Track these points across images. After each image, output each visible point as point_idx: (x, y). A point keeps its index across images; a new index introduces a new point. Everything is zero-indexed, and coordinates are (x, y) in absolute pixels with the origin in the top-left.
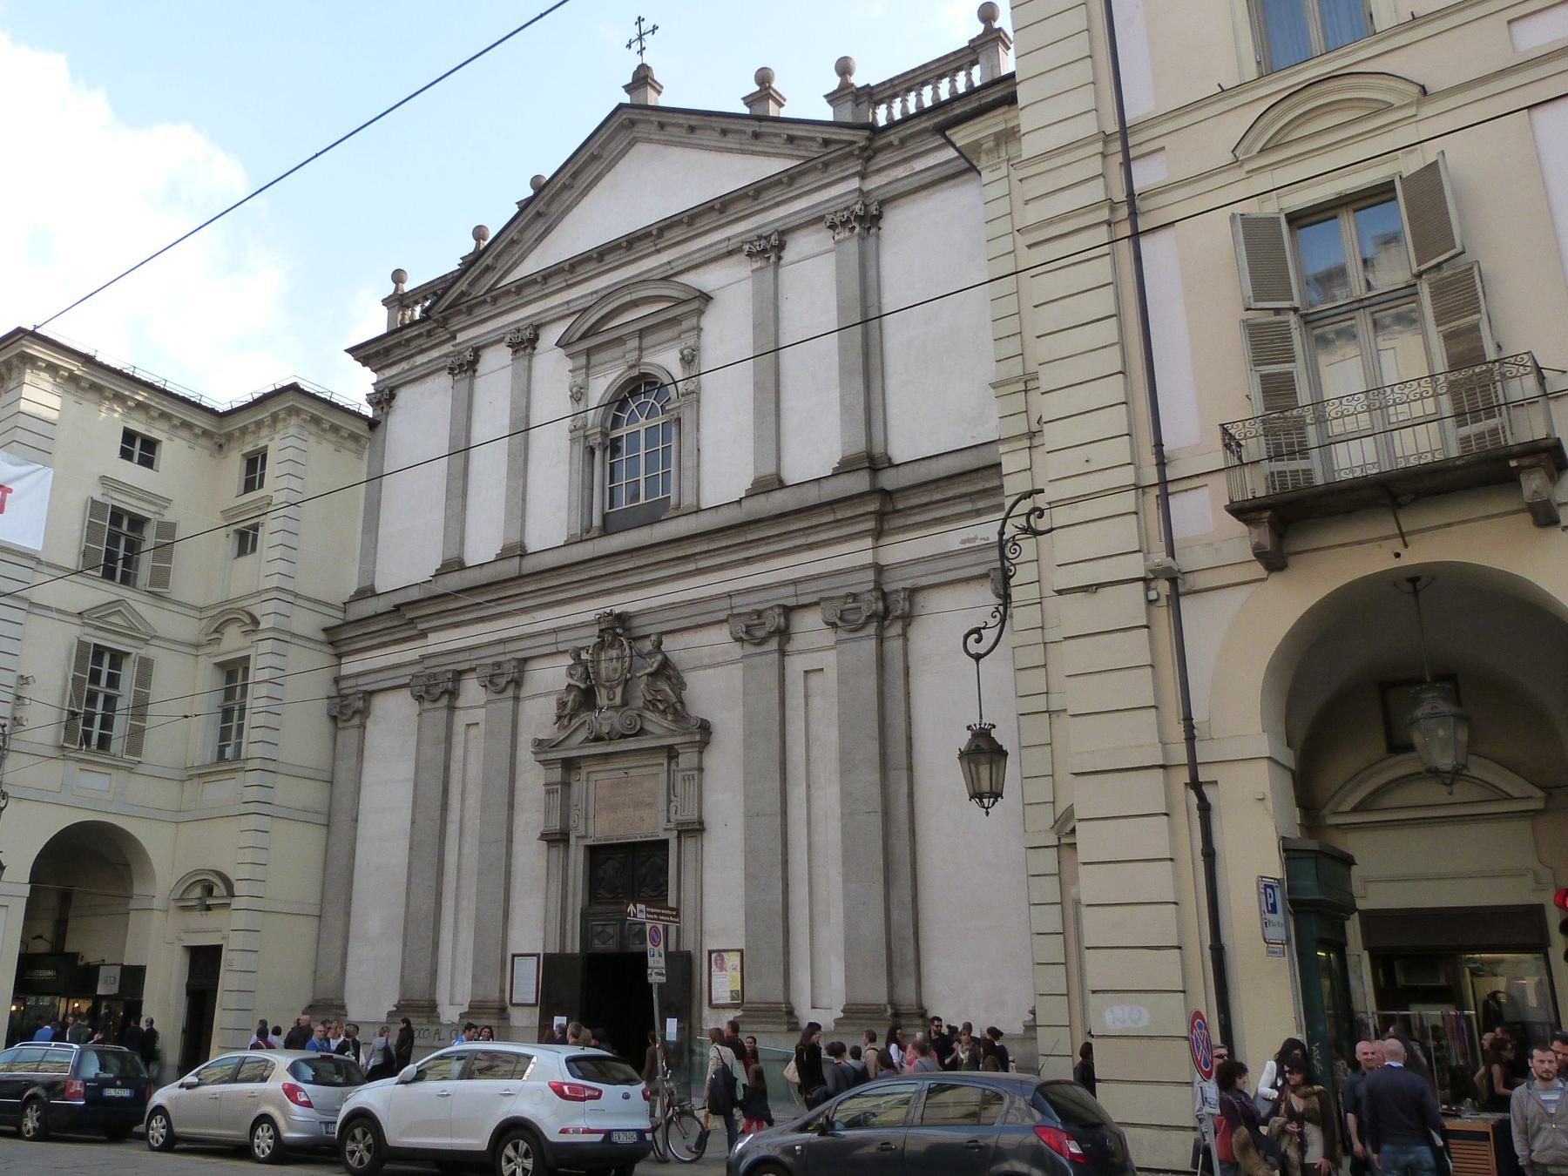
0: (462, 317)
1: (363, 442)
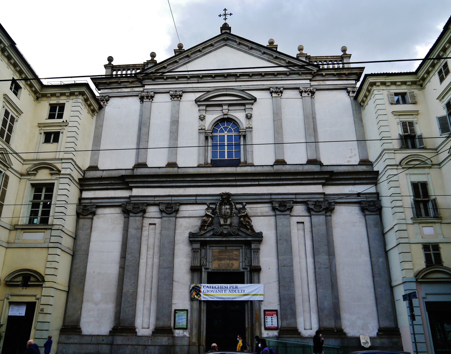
1: (95, 113)
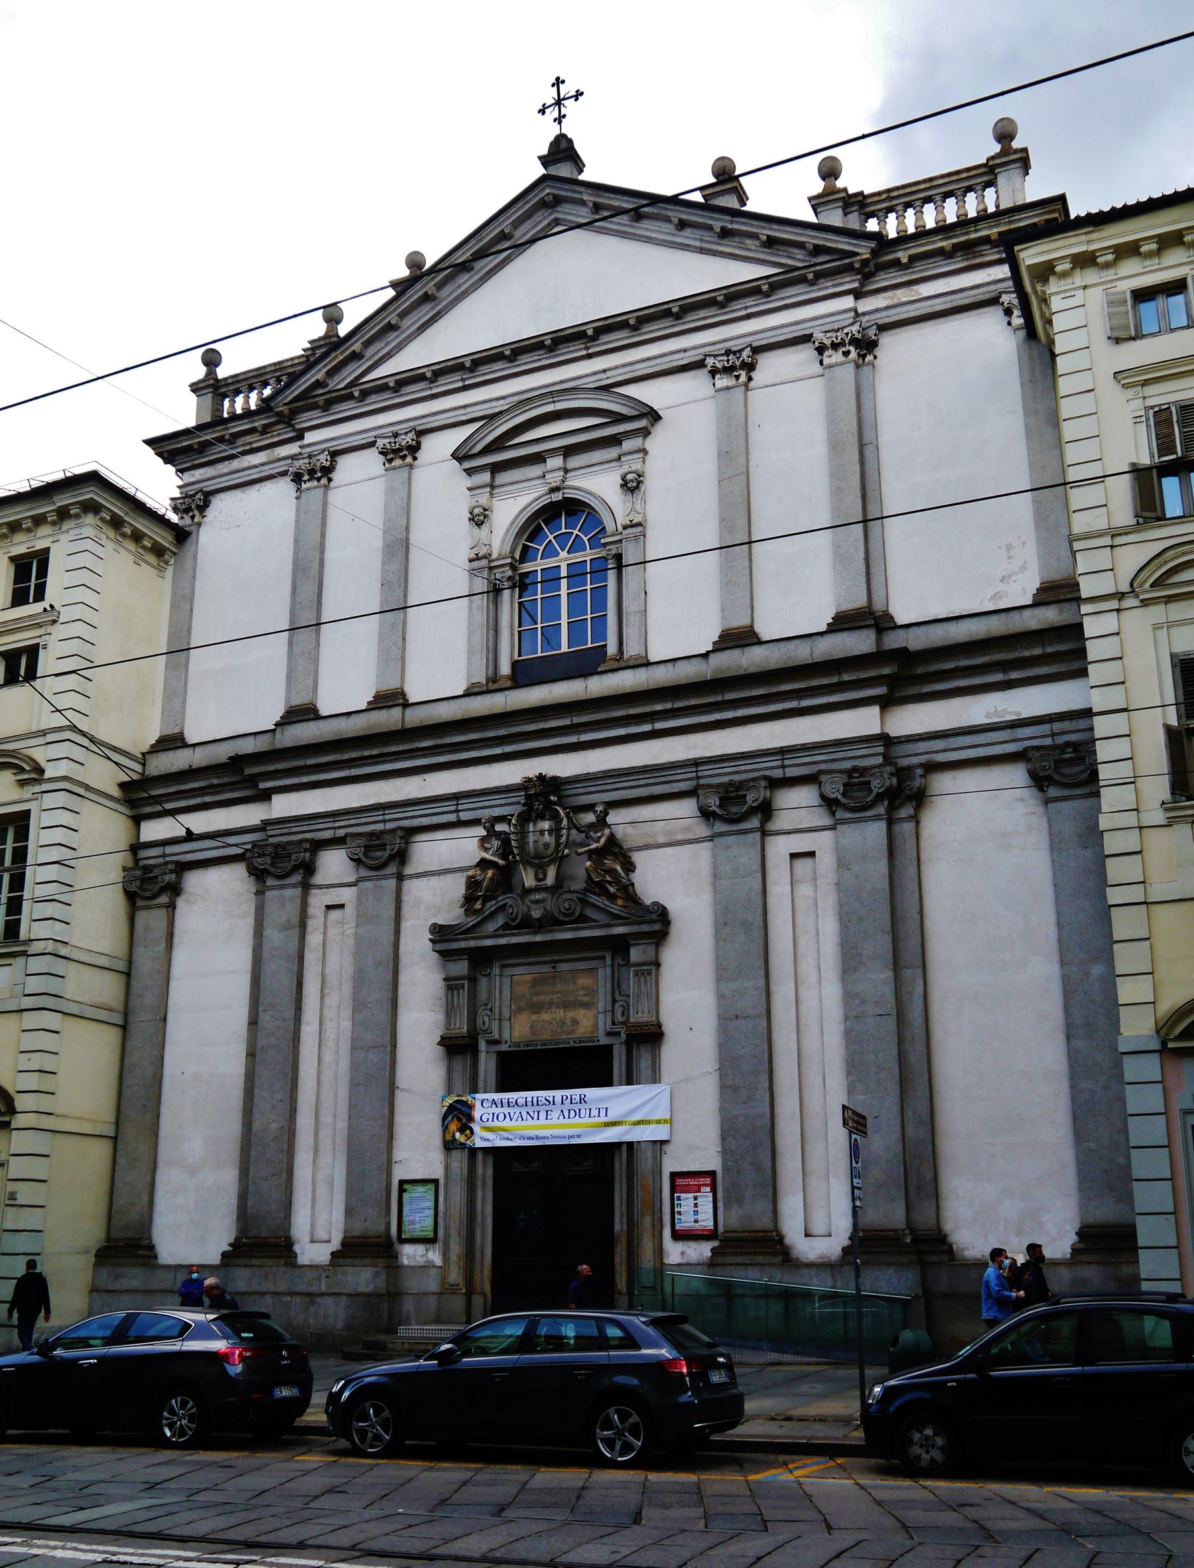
0: (315, 413)
1: (167, 557)
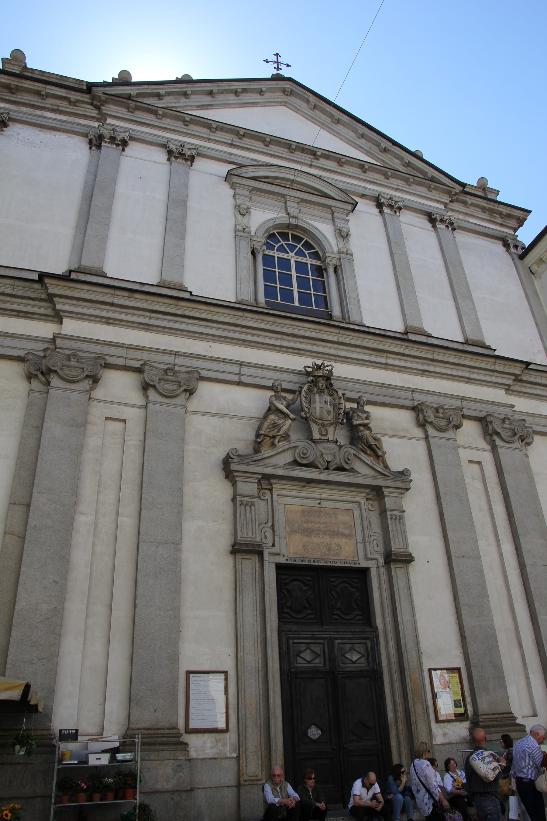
0: (124, 110)
